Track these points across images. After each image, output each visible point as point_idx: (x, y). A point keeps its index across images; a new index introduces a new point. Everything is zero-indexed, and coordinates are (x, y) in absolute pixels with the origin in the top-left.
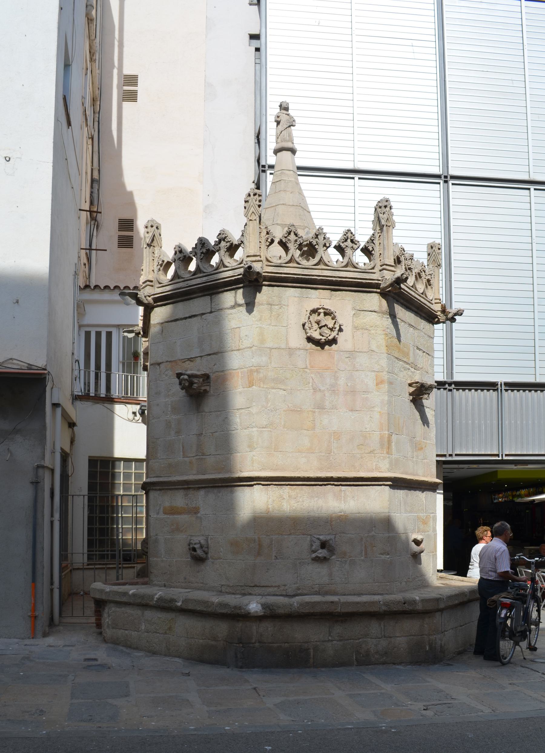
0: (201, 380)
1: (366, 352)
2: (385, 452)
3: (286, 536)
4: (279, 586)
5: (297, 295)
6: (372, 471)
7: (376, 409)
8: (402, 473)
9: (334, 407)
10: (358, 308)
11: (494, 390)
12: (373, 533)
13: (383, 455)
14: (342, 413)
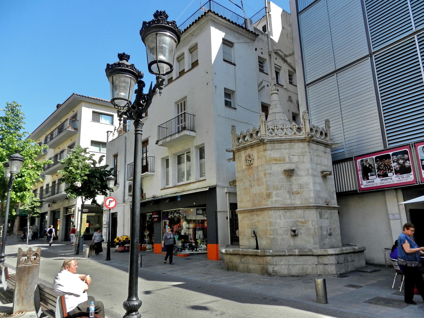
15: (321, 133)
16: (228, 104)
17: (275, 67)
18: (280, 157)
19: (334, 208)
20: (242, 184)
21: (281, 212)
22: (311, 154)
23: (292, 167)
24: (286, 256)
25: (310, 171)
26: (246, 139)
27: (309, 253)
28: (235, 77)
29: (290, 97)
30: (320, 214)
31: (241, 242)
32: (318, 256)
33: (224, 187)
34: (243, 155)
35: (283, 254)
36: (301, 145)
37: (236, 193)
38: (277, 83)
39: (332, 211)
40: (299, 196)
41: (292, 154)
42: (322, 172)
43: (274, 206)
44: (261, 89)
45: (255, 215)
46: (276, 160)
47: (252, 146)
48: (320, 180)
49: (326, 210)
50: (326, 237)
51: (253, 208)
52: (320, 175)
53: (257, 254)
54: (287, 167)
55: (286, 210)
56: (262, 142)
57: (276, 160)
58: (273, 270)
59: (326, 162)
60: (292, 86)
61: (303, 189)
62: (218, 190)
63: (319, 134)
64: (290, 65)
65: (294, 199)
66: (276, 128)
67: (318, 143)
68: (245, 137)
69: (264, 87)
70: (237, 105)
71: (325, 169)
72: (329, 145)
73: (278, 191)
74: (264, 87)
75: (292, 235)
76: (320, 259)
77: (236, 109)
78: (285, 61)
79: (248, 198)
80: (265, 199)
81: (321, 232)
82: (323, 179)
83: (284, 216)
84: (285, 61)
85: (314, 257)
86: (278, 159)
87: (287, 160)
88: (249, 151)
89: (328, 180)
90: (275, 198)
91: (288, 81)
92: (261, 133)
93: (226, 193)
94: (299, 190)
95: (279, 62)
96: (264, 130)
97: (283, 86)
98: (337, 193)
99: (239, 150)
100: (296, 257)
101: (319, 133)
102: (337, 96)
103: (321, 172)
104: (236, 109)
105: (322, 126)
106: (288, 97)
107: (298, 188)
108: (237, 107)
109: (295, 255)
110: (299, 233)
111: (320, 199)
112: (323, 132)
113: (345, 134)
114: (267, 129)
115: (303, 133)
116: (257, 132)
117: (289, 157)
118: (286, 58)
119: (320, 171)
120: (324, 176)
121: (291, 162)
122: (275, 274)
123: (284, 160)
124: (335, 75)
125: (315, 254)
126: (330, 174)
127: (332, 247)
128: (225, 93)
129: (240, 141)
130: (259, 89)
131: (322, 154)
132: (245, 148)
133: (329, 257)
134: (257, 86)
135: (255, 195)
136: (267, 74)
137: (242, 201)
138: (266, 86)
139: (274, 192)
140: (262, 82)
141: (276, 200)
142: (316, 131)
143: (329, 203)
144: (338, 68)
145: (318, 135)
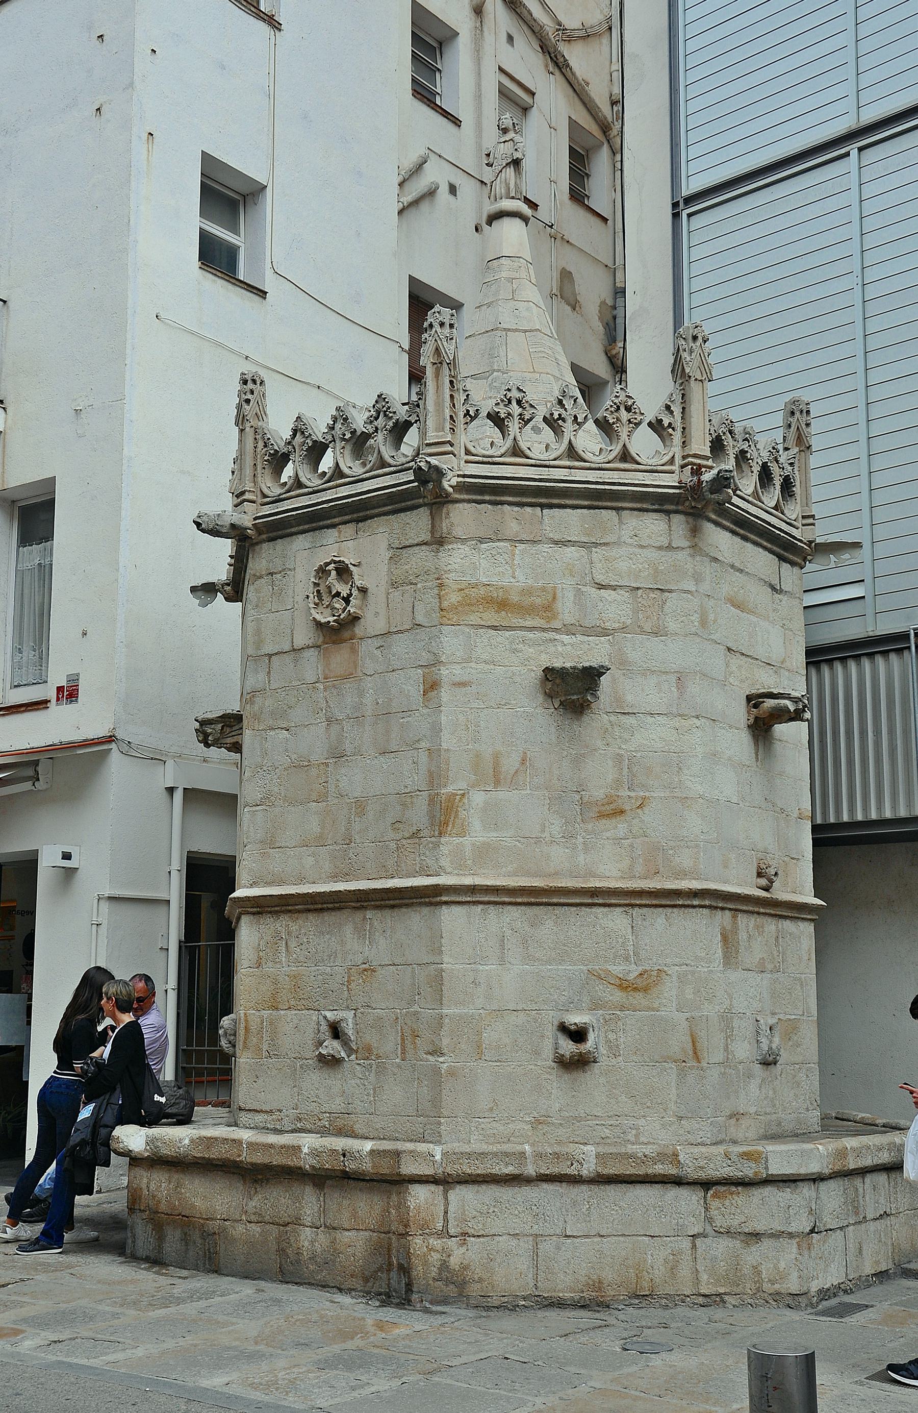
1: (407, 630)
5: (307, 545)
6: (682, 874)
7: (423, 744)
8: (515, 874)
9: (358, 752)
11: (899, 651)
12: (416, 1008)
13: (433, 839)
15: (765, 476)
16: (217, 258)
17: (503, 92)
18: (527, 592)
19: (796, 910)
22: (705, 587)
27: (659, 1169)
29: (566, 276)
30: (725, 938)
31: (245, 1088)
32: (706, 1185)
33: (158, 759)
34: (303, 556)
35: (510, 1170)
36: (652, 526)
39: (787, 925)
40: (620, 827)
41: (600, 578)
42: (754, 700)
43: (468, 881)
44: (415, 203)
45: (348, 930)
46: (502, 605)
47: (359, 512)
49: (760, 920)
51: (341, 886)
53: (351, 1166)
54: (570, 653)
55: (536, 910)
56: (425, 492)
57: (502, 605)
58: (444, 1265)
60: (581, 213)
63: (755, 477)
64: (577, 90)
65: (586, 848)
66: (515, 409)
67: (745, 527)
68: (316, 451)
69: (431, 193)
70: (269, 273)
71: (767, 681)
73: (502, 795)
74: (431, 193)
76: (715, 1204)
77: (262, 294)
78: (559, 64)
79: (314, 826)
80: (416, 835)
83: (525, 942)
84: (559, 64)
85: (683, 1193)
86: (515, 598)
87: (567, 610)
88: (336, 545)
89: (777, 746)
90: (478, 833)
92: (423, 433)
93: (171, 790)
95: (526, 63)
96: (448, 413)
99: (277, 529)
100: (583, 1191)
101: (756, 469)
102: (852, 281)
103: (749, 698)
104: (262, 294)
105: (767, 434)
106: (556, 275)
107: (618, 782)
108: (269, 283)
109: (575, 1180)
110: (603, 1050)
112: (774, 468)
113: (880, 498)
115: (672, 461)
116: (399, 430)
117: (579, 593)
118: (563, 48)
122: (452, 1290)
123: (548, 609)
124: (854, 153)
125: (692, 1173)
126: (797, 716)
128: (207, 192)
129: (288, 472)
131: (760, 596)
132: (315, 520)
133: (767, 1191)
135: (360, 807)
136: (457, 122)
137: (270, 843)
138: (444, 189)
139: (478, 798)
140: (419, 168)
141: (487, 842)
142: (742, 457)
144: (870, 115)
145: (748, 484)
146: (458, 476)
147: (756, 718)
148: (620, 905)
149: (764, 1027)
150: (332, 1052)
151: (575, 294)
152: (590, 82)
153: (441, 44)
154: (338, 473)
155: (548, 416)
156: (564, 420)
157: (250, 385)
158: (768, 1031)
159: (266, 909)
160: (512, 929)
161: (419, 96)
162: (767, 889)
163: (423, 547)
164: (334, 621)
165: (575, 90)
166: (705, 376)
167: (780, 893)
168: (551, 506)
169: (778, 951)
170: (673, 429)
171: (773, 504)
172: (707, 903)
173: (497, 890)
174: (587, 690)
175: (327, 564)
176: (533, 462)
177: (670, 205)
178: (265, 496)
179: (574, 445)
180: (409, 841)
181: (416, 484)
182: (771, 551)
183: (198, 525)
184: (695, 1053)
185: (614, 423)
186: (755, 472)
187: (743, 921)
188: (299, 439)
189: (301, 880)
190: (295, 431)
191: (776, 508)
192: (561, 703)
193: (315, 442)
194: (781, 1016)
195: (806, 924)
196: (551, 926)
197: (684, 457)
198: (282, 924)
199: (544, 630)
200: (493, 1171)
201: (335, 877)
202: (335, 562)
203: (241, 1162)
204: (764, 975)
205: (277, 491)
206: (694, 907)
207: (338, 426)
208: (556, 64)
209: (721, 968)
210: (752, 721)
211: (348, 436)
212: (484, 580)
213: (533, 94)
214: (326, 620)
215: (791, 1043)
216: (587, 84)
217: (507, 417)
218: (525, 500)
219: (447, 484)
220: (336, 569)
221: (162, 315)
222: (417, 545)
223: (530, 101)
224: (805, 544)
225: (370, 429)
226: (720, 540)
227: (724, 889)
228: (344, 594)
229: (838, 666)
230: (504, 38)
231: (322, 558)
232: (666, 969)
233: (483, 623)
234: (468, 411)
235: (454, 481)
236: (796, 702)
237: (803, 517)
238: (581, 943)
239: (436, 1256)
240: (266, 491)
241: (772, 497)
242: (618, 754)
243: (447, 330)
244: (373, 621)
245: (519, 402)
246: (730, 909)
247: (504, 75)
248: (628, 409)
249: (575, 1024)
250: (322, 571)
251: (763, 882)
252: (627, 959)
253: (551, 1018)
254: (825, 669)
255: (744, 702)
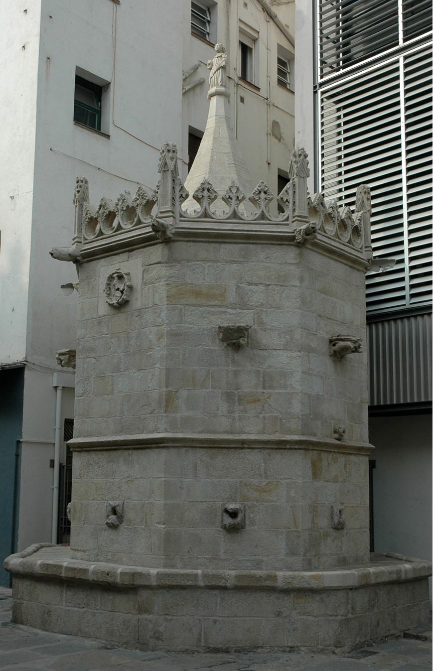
0: (67, 356)
2: (163, 411)
3: (91, 501)
4: (85, 551)
10: (147, 263)
14: (132, 374)
17: (241, 31)
19: (360, 450)
20: (93, 360)
21: (201, 455)
23: (244, 319)
24: (199, 587)
25: (298, 335)
26: (115, 224)
28: (115, 39)
29: (275, 124)
34: (104, 268)
37: (74, 388)
38: (244, 77)
39: (352, 458)
42: (332, 342)
44: (193, 88)
46: (198, 294)
47: (128, 247)
48: (323, 363)
50: (326, 535)
52: (325, 348)
55: (213, 451)
59: (351, 317)
61: (271, 387)
62: (27, 374)
64: (283, 31)
66: (206, 193)
68: (111, 216)
71: (343, 331)
72: (360, 264)
75: (224, 527)
81: (313, 522)
82: (334, 361)
87: (232, 297)
91: (275, 76)
93: (56, 388)
94: (260, 390)
96: (170, 197)
97: (258, 89)
98: (370, 408)
103: (331, 341)
106: (270, 124)
108: (112, 131)
109: (225, 588)
110: (247, 522)
111: (319, 423)
114: (178, 194)
117: (238, 287)
119: (328, 337)
120: (339, 352)
121: (243, 305)
126: (356, 350)
127: (343, 563)
130: (187, 88)
134: (181, 78)
140: (196, 69)
143: (346, 436)
145: (331, 229)
146: (176, 228)
147: (335, 351)
148: (257, 448)
149: (336, 511)
150: (113, 522)
151: (280, 134)
152: (289, 25)
153: (209, 9)
154: (119, 227)
155: (224, 197)
156: (231, 199)
157: (80, 183)
158: (338, 513)
159: (84, 449)
160: (201, 460)
161: (195, 35)
162: (339, 440)
163: (159, 265)
164: (116, 303)
165: (281, 30)
166: (305, 175)
167: (348, 441)
168: (225, 243)
169: (346, 471)
170: (289, 202)
171: (347, 240)
172: (303, 447)
173: (193, 440)
174: (241, 337)
175: (113, 274)
176: (215, 220)
177: (312, 87)
178: (86, 240)
179: (237, 211)
180: (151, 415)
181: (153, 233)
182: (346, 265)
183: (52, 254)
184: (295, 524)
185: (258, 200)
186: (337, 224)
187: (324, 456)
188: (102, 210)
189: (100, 434)
190: (100, 207)
191: (349, 242)
192: (228, 344)
193: (110, 212)
194: (347, 505)
195: (364, 457)
196: (221, 459)
197: (294, 217)
198: (94, 457)
199: (219, 306)
200: (181, 584)
201: (115, 433)
202: (117, 273)
203: (61, 576)
204: (337, 484)
205: (92, 237)
206: (296, 449)
207: (120, 203)
208: (271, 17)
209: (311, 480)
210: (332, 352)
211: (125, 208)
212: (189, 281)
213: (258, 32)
214: (112, 302)
215: (353, 519)
216: (288, 27)
217: (202, 198)
218: (210, 240)
219: (169, 234)
220: (118, 276)
221: (54, 149)
222: (155, 264)
223: (255, 35)
224: (366, 261)
225: (135, 204)
226: (317, 260)
227: (188, 437)
228: (121, 289)
229: (392, 323)
230: (242, 4)
231: (111, 270)
232: (281, 481)
233: (188, 303)
234: (182, 195)
235: (173, 231)
236: (355, 343)
237: (366, 247)
238: (236, 468)
239: (151, 626)
240: (86, 237)
241: (347, 235)
242: (257, 370)
243: (171, 154)
244: (137, 302)
245: (208, 190)
246: (316, 450)
247: (241, 23)
248: (265, 193)
249: (232, 509)
250: (111, 278)
251: (337, 436)
252: (260, 475)
253: (219, 504)
254: (386, 325)
255: (328, 342)
